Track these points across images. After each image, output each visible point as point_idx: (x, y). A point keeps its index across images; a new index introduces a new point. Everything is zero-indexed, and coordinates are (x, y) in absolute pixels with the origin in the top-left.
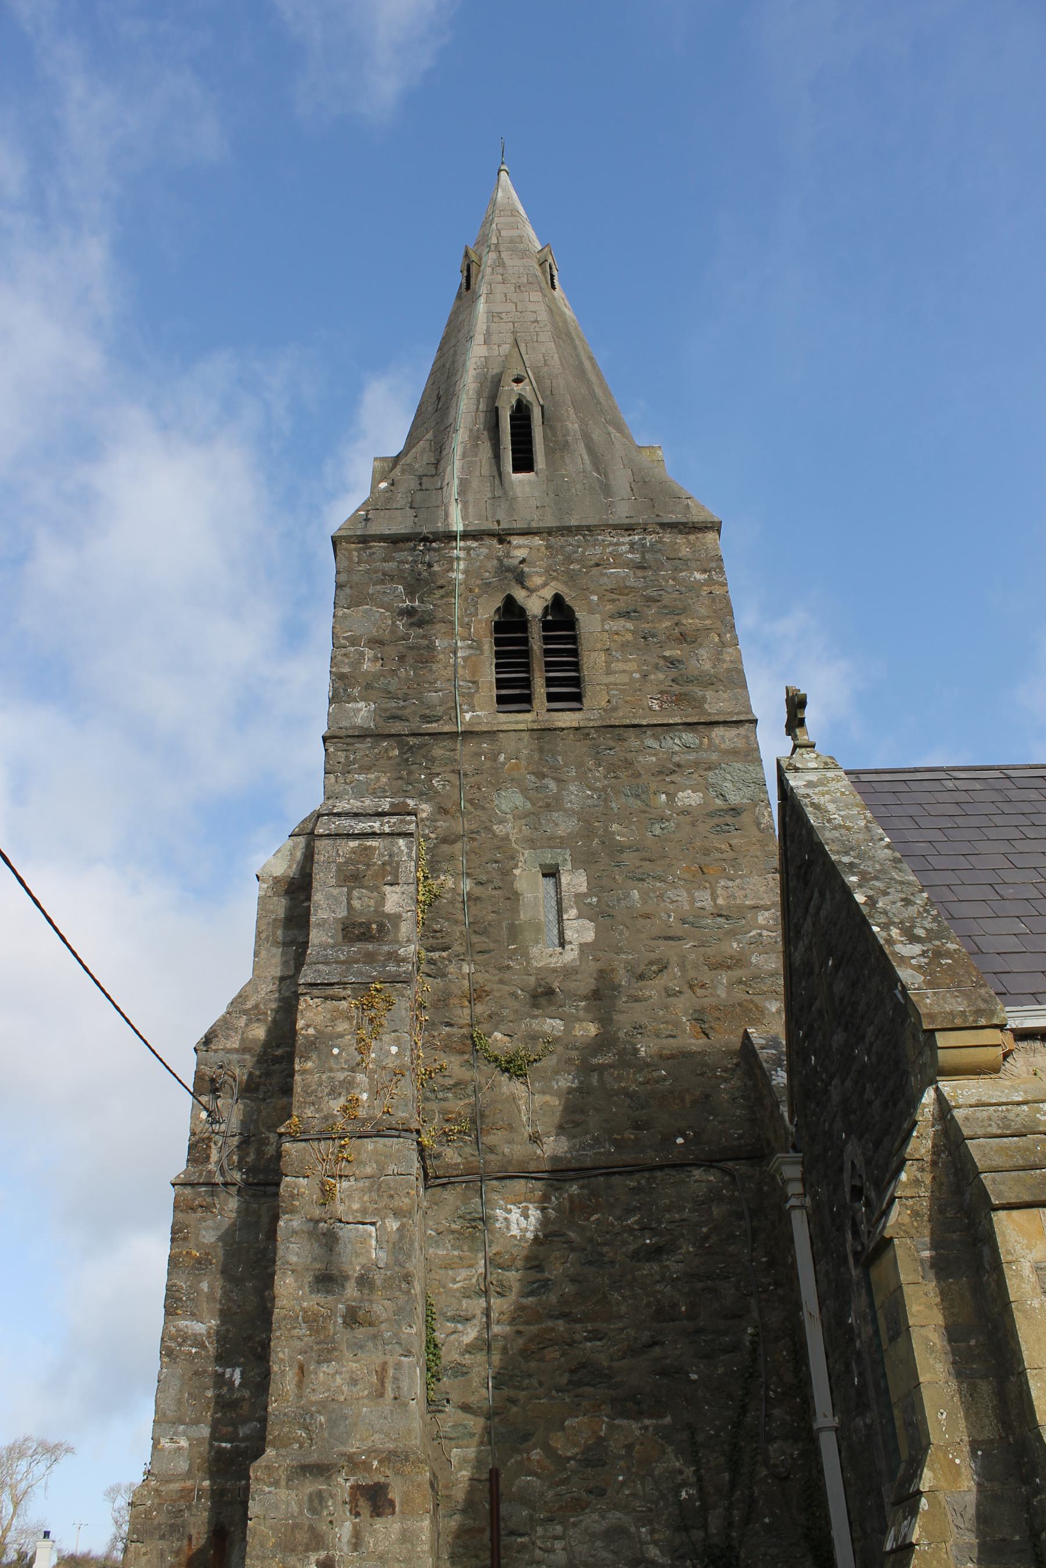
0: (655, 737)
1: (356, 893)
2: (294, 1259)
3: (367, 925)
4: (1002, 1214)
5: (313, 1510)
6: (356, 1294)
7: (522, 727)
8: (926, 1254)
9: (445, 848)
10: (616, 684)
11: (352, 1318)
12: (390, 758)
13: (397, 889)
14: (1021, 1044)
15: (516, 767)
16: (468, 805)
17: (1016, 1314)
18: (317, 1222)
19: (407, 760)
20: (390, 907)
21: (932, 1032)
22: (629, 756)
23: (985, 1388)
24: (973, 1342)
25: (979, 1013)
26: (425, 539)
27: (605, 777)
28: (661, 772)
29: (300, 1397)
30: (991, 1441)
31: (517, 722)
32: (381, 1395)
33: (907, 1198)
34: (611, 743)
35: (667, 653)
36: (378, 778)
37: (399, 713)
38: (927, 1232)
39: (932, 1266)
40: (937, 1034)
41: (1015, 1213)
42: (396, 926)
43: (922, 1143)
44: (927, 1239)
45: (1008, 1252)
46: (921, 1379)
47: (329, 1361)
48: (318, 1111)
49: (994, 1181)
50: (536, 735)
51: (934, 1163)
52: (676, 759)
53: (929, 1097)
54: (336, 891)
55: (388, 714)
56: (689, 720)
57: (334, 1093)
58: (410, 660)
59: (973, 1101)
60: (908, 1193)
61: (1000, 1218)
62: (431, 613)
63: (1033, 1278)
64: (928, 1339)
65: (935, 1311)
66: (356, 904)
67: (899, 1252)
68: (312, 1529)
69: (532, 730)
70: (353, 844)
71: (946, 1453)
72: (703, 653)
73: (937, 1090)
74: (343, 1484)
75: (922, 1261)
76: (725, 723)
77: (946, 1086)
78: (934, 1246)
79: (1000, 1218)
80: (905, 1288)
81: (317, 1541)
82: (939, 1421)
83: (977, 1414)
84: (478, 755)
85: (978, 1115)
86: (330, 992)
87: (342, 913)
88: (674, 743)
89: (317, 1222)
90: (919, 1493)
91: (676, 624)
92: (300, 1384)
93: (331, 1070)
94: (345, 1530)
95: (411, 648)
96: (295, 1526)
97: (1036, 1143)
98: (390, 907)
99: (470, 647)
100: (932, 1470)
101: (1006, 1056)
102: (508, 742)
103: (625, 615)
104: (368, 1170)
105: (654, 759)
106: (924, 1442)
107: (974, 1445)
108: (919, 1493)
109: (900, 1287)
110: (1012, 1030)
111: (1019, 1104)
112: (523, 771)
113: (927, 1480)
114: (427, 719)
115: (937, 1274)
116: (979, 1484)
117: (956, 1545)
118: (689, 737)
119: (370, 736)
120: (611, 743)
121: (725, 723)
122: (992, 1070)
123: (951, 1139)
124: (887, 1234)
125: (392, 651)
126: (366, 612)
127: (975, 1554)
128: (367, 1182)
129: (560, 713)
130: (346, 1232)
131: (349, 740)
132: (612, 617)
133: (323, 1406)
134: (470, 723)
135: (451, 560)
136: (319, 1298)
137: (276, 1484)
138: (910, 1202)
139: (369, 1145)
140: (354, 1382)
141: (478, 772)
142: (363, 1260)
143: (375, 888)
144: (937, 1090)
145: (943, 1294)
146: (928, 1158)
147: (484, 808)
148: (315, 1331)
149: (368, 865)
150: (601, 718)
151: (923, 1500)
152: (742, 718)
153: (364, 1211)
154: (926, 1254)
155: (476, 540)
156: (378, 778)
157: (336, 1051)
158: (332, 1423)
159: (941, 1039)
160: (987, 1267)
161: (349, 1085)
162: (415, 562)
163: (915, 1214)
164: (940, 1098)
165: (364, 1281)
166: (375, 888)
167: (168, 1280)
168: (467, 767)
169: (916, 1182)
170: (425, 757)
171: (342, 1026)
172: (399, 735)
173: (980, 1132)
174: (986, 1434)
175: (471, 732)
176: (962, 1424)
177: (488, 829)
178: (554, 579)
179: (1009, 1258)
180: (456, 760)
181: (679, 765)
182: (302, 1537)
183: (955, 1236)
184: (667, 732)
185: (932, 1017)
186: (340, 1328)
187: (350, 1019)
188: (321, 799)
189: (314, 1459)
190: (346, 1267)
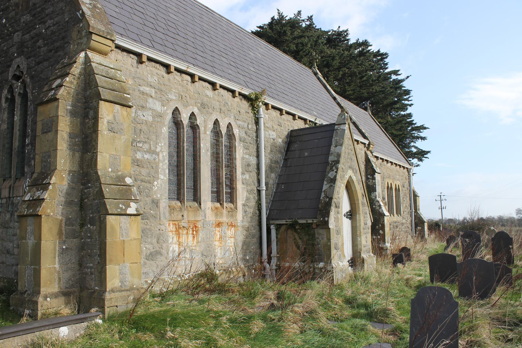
4: (103, 102)
8: (69, 107)
14: (116, 50)
17: (99, 135)
21: (92, 33)
23: (77, 155)
24: (77, 140)
25: (108, 33)
30: (75, 171)
33: (67, 87)
38: (71, 100)
39: (70, 112)
40: (93, 35)
41: (106, 103)
43: (76, 69)
44: (70, 103)
45: (101, 115)
46: (58, 148)
49: (102, 91)
51: (79, 78)
53: (82, 55)
59: (98, 62)
60: (68, 85)
61: (102, 103)
63: (106, 125)
64: (63, 135)
65: (68, 127)
67: (60, 104)
71: (61, 173)
73: (86, 53)
75: (67, 110)
77: (90, 54)
78: (73, 106)
79: (102, 103)
80: (60, 117)
82: (61, 162)
83: (73, 162)
85: (99, 67)
90: (49, 184)
97: (116, 83)
100: (56, 177)
101: (111, 51)
106: (52, 168)
107: (70, 171)
108: (49, 184)
109: (58, 116)
110: (115, 43)
111: (111, 68)
113: (53, 180)
115: (71, 115)
116: (69, 183)
117: (58, 200)
123: (88, 73)
124: (58, 97)
127: (63, 204)
138: (68, 88)
144: (86, 53)
145: (71, 122)
146: (77, 76)
151: (51, 186)
154: (69, 107)
159: (94, 37)
160: (90, 117)
163: (69, 93)
164: (86, 56)
167: (310, 65)
169: (71, 83)
173: (100, 73)
174: (74, 169)
176: (68, 164)
179: (101, 117)
183: (79, 104)
185: (93, 28)
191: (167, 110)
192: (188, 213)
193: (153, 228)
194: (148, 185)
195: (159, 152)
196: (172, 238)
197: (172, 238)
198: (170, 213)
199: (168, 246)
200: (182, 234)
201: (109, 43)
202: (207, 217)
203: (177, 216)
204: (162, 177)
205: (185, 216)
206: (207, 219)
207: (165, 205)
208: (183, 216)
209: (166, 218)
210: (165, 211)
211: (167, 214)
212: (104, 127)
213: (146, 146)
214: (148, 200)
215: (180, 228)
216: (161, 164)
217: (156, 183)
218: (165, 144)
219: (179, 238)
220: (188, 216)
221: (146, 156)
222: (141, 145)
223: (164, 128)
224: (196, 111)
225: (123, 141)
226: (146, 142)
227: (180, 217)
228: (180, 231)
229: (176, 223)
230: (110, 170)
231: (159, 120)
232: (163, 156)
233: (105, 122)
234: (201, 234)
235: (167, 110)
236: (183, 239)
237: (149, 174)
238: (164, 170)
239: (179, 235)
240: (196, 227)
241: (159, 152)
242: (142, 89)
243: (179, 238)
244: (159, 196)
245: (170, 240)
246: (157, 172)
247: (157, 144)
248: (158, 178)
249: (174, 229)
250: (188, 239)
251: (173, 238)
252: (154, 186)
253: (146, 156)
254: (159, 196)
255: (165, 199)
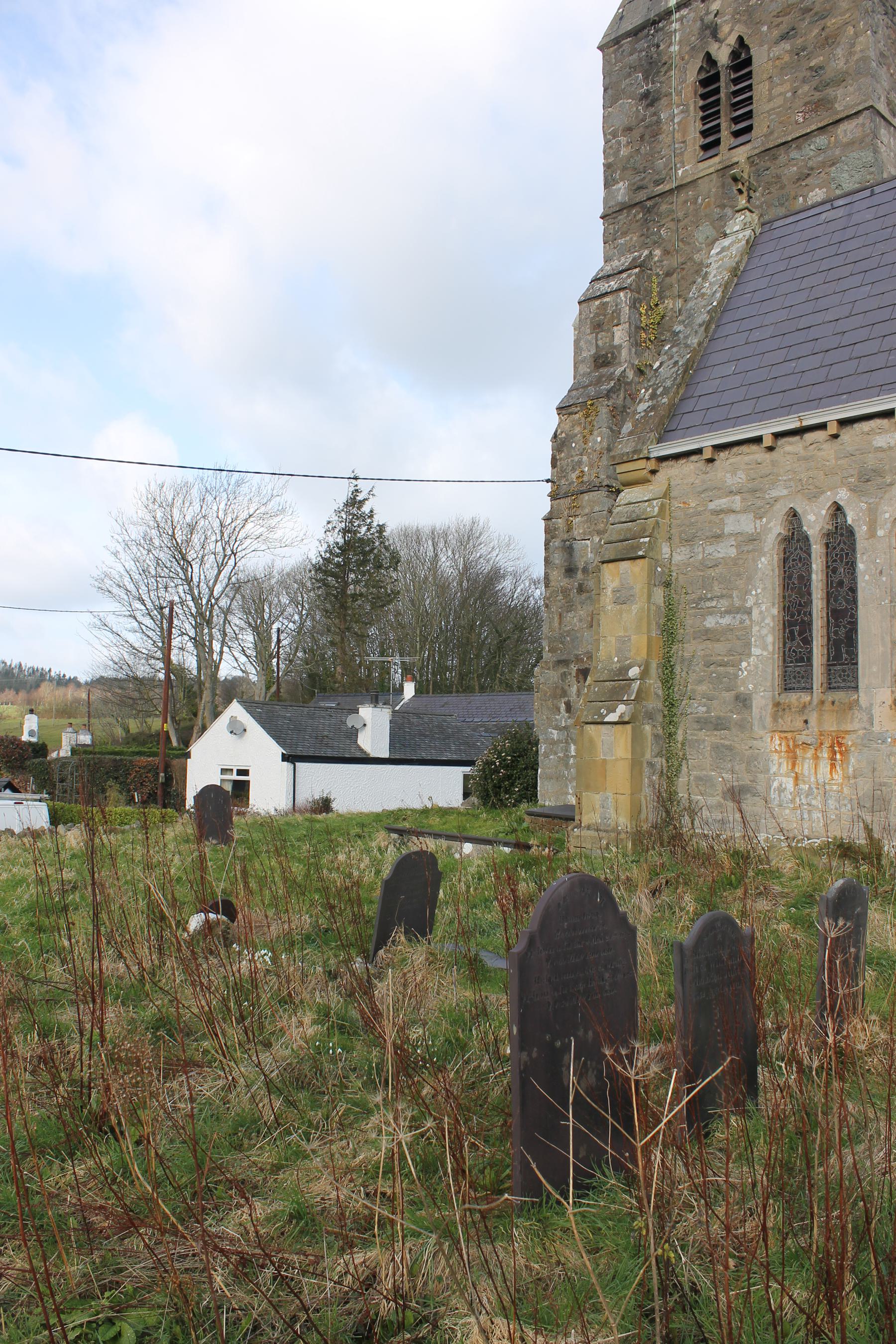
0: (799, 148)
1: (599, 336)
2: (557, 562)
3: (606, 356)
5: (562, 680)
6: (582, 577)
7: (712, 170)
9: (668, 280)
10: (774, 109)
11: (581, 589)
12: (637, 221)
13: (620, 327)
15: (709, 203)
16: (680, 244)
18: (565, 541)
19: (647, 220)
20: (617, 341)
22: (778, 171)
26: (654, 23)
27: (763, 195)
28: (798, 180)
29: (560, 629)
31: (709, 167)
32: (592, 626)
34: (768, 164)
35: (812, 64)
36: (631, 239)
37: (641, 183)
42: (620, 352)
47: (571, 611)
48: (567, 480)
50: (720, 174)
52: (810, 163)
54: (589, 337)
55: (636, 186)
56: (820, 125)
57: (574, 470)
58: (647, 137)
62: (658, 91)
66: (600, 343)
68: (563, 688)
69: (718, 171)
70: (597, 303)
72: (839, 52)
74: (574, 668)
76: (848, 117)
81: (564, 693)
84: (686, 202)
86: (570, 410)
87: (593, 351)
88: (809, 149)
89: (565, 541)
91: (823, 29)
92: (560, 624)
93: (572, 456)
94: (574, 689)
95: (647, 127)
96: (557, 687)
98: (617, 341)
99: (682, 112)
102: (703, 186)
103: (784, 37)
104: (587, 511)
105: (795, 168)
112: (713, 206)
114: (658, 183)
118: (821, 140)
119: (624, 208)
120: (768, 164)
121: (848, 117)
122: (644, 481)
125: (636, 133)
126: (620, 106)
128: (585, 518)
129: (737, 149)
130: (577, 545)
131: (614, 215)
132: (777, 43)
133: (568, 633)
134: (683, 177)
135: (670, 34)
136: (567, 580)
137: (549, 669)
139: (586, 497)
140: (581, 620)
141: (686, 215)
142: (585, 559)
143: (608, 330)
147: (689, 244)
148: (565, 597)
149: (605, 315)
150: (763, 144)
152: (860, 108)
153: (584, 533)
155: (687, 7)
156: (631, 239)
157: (574, 445)
158: (572, 640)
161: (580, 463)
162: (648, 47)
165: (585, 570)
166: (608, 330)
168: (680, 214)
170: (656, 214)
171: (577, 429)
172: (641, 202)
175: (681, 186)
177: (691, 259)
178: (739, 21)
180: (673, 211)
181: (812, 169)
182: (559, 692)
184: (807, 139)
186: (576, 595)
187: (580, 424)
188: (601, 263)
189: (563, 658)
190: (578, 563)
191: (768, 522)
192: (821, 715)
193: (737, 745)
194: (731, 670)
195: (751, 608)
196: (778, 765)
197: (778, 765)
198: (775, 718)
199: (769, 779)
200: (804, 759)
201: (642, 464)
202: (876, 721)
203: (792, 721)
204: (756, 651)
205: (813, 721)
206: (876, 728)
207: (763, 702)
208: (806, 722)
209: (764, 728)
210: (764, 713)
211: (768, 720)
212: (608, 600)
213: (724, 604)
214: (728, 696)
215: (796, 746)
216: (755, 629)
217: (744, 664)
218: (764, 589)
219: (794, 765)
220: (820, 722)
221: (726, 621)
222: (714, 603)
223: (763, 559)
224: (843, 496)
225: (634, 613)
226: (722, 596)
227: (799, 724)
228: (798, 752)
229: (789, 735)
230: (616, 659)
231: (751, 547)
232: (761, 612)
233: (609, 593)
234: (853, 760)
235: (768, 522)
236: (806, 767)
237: (730, 652)
238: (763, 638)
239: (794, 760)
240: (840, 745)
241: (751, 608)
242: (712, 506)
243: (794, 765)
244: (751, 686)
245: (774, 769)
246: (748, 645)
247: (748, 592)
248: (749, 655)
249: (784, 748)
250: (818, 770)
251: (780, 764)
252: (740, 669)
253: (726, 621)
254: (751, 686)
255: (765, 691)
